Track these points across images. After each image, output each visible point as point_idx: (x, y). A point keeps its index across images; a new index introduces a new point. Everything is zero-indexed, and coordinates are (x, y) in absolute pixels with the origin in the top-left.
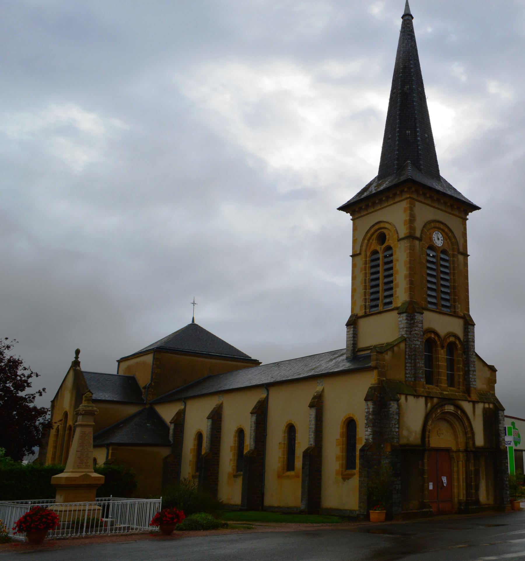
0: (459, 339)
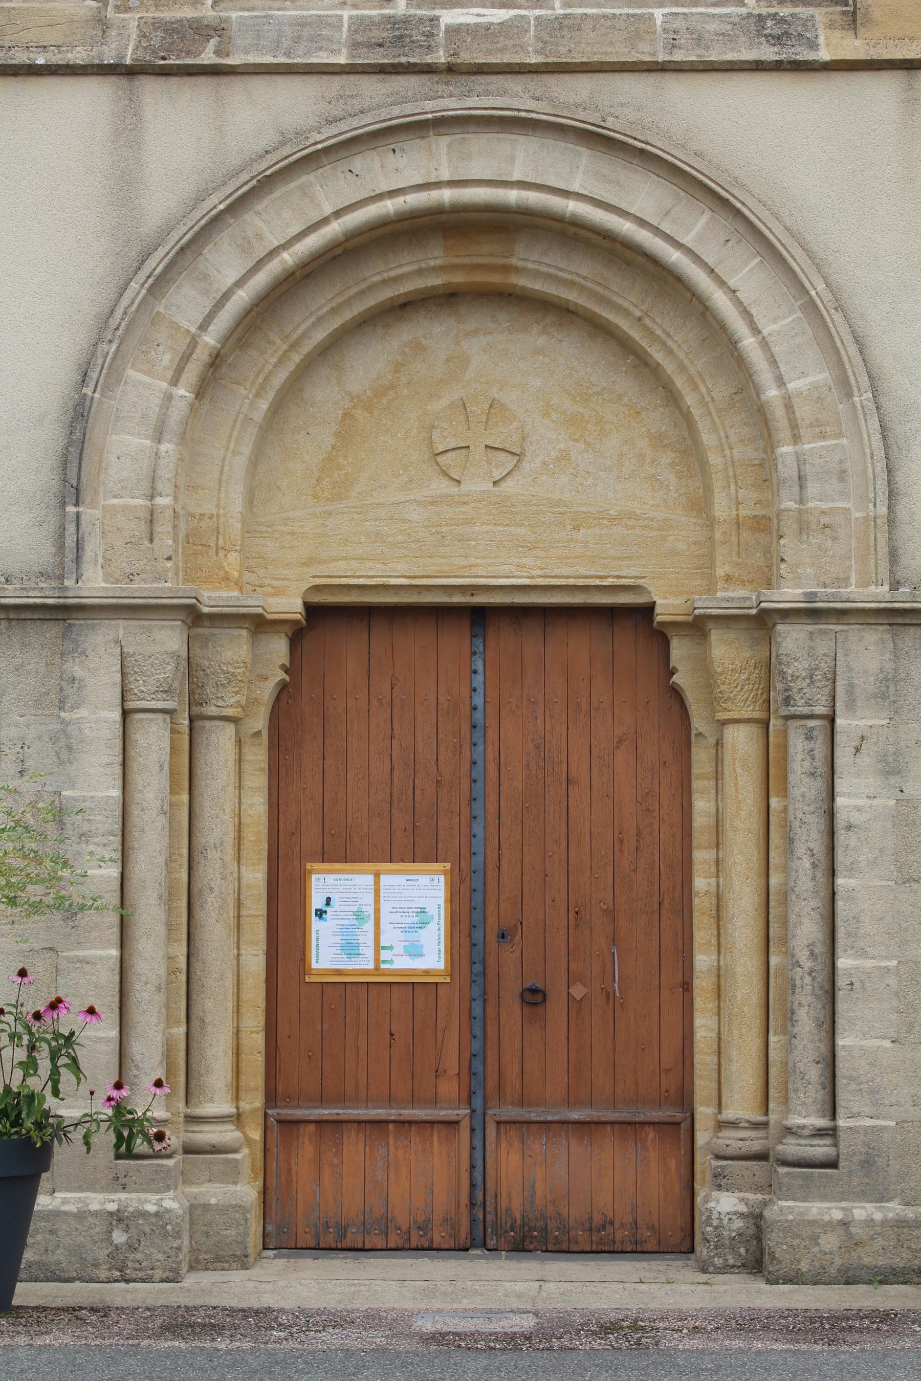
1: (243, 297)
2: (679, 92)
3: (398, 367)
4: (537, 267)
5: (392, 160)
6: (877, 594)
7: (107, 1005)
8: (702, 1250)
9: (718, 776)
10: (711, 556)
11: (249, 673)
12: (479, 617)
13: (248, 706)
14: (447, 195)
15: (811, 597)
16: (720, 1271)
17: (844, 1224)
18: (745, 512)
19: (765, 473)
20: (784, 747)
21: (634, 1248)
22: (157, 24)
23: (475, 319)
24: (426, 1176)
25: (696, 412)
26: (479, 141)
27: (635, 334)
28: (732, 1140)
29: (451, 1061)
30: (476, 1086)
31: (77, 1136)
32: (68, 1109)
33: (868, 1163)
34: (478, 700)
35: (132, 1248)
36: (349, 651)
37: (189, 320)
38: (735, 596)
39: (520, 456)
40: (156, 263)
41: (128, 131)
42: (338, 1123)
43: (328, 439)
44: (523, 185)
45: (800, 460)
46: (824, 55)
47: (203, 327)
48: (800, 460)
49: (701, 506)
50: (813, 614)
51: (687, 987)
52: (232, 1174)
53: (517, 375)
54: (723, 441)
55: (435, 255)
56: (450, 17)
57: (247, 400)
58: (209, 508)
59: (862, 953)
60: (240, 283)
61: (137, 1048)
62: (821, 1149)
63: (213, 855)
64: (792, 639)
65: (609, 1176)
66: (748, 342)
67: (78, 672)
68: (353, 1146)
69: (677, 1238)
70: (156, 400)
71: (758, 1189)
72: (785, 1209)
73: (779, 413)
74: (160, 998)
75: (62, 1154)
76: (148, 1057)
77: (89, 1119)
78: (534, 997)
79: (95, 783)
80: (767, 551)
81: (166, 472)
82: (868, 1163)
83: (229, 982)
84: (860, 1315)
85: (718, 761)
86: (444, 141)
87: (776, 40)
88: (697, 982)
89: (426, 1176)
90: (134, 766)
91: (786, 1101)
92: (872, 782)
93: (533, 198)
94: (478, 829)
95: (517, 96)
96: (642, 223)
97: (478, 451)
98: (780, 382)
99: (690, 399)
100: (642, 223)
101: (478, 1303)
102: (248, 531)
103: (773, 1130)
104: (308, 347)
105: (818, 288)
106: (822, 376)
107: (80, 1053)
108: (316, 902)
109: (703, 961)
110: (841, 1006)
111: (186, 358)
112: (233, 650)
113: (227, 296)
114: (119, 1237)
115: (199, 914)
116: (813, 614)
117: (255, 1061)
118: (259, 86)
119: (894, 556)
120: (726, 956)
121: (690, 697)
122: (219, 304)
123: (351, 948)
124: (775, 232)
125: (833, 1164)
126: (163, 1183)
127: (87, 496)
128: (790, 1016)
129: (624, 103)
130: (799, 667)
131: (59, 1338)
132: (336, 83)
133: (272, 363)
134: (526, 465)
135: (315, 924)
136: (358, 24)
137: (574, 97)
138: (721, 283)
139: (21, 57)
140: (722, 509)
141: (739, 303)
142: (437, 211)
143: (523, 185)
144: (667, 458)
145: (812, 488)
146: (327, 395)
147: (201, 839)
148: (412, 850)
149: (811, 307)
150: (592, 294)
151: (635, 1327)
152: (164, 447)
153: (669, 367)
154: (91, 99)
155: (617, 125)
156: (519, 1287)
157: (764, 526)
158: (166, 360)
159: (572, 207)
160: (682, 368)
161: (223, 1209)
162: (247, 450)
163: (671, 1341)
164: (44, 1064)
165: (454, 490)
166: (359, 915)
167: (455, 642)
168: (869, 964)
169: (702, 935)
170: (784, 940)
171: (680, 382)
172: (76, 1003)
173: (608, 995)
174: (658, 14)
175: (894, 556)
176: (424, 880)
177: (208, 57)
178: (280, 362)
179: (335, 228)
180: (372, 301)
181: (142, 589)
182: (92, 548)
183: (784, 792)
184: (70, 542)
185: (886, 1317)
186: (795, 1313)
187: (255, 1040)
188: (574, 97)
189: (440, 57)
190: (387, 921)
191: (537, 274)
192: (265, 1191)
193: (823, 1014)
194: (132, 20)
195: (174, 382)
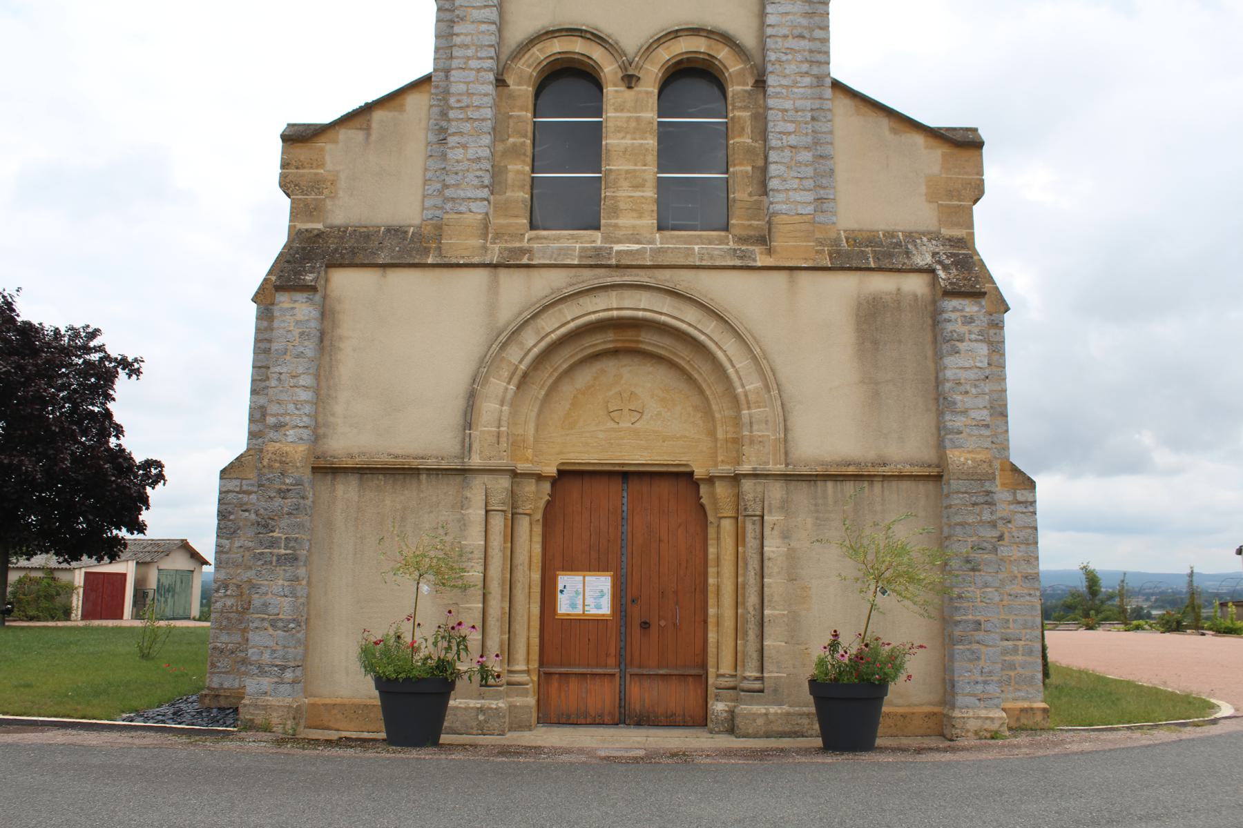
0: (726, 39)
1: (536, 350)
2: (704, 275)
3: (595, 379)
4: (650, 341)
5: (594, 300)
6: (780, 468)
7: (479, 624)
8: (710, 725)
9: (718, 539)
10: (716, 452)
11: (536, 496)
12: (625, 476)
13: (535, 509)
14: (615, 313)
15: (755, 469)
16: (717, 733)
17: (766, 714)
18: (729, 436)
19: (737, 421)
20: (744, 528)
21: (684, 724)
22: (506, 249)
23: (625, 360)
24: (602, 695)
25: (710, 397)
26: (627, 293)
27: (687, 367)
28: (722, 682)
29: (612, 650)
30: (622, 660)
31: (466, 677)
32: (462, 667)
33: (775, 690)
34: (625, 508)
35: (486, 721)
36: (574, 489)
37: (515, 360)
38: (725, 469)
39: (642, 413)
40: (503, 338)
41: (494, 288)
42: (567, 674)
43: (568, 406)
44: (644, 310)
45: (750, 416)
46: (759, 264)
47: (520, 362)
48: (750, 416)
49: (712, 433)
50: (756, 476)
51: (705, 622)
52: (525, 693)
53: (641, 382)
54: (721, 409)
55: (610, 336)
56: (617, 247)
57: (537, 390)
58: (521, 432)
59: (774, 608)
60: (535, 346)
61: (489, 643)
62: (757, 685)
63: (520, 568)
64: (747, 485)
65: (675, 696)
66: (731, 371)
67: (469, 495)
68: (573, 684)
69: (701, 720)
70: (502, 390)
71: (732, 701)
72: (743, 708)
73: (742, 398)
74: (498, 624)
75: (458, 683)
76: (494, 645)
77: (470, 670)
78: (645, 625)
79: (475, 539)
80: (738, 451)
81: (504, 418)
82: (775, 690)
83: (526, 618)
84: (772, 750)
85: (718, 533)
86: (614, 293)
87: (741, 258)
88: (709, 620)
89: (602, 695)
90: (490, 532)
91: (744, 666)
92: (778, 541)
93: (648, 315)
94: (624, 559)
95: (630, 277)
96: (690, 325)
97: (626, 411)
98: (743, 386)
99: (708, 392)
100: (690, 325)
101: (623, 745)
102: (536, 440)
103: (739, 678)
104: (561, 370)
105: (757, 351)
106: (759, 384)
107: (469, 644)
108: (560, 587)
109: (712, 611)
110: (765, 629)
111: (513, 374)
112: (529, 487)
113: (530, 350)
114: (481, 717)
115: (514, 591)
116: (756, 476)
117: (535, 649)
118: (544, 271)
119: (786, 454)
120: (721, 610)
121: (708, 508)
122: (527, 354)
123: (573, 606)
124: (741, 330)
125: (762, 691)
126: (497, 696)
127: (474, 426)
128: (746, 633)
129: (683, 281)
130: (750, 496)
131: (458, 756)
132: (574, 270)
133: (546, 376)
134: (644, 417)
135: (560, 596)
136: (583, 249)
137: (664, 278)
138: (720, 348)
139: (454, 261)
140: (720, 434)
141: (727, 356)
142: (611, 319)
143: (644, 310)
144: (699, 415)
145: (755, 427)
146: (567, 389)
147: (516, 562)
148: (596, 566)
149: (754, 358)
150: (670, 351)
151: (684, 754)
152: (504, 408)
153: (700, 380)
154: (481, 275)
155: (681, 288)
156: (639, 739)
157: (737, 441)
158: (506, 374)
159: (663, 318)
160: (705, 380)
161: (521, 707)
162: (536, 410)
163: (699, 760)
164: (455, 648)
165: (616, 426)
166: (577, 592)
167: (616, 486)
168: (776, 612)
169: (712, 601)
170: (744, 603)
171: (704, 386)
172: (468, 622)
173: (675, 624)
174: (696, 247)
175: (786, 454)
176: (603, 579)
177: (525, 261)
178: (550, 375)
179: (572, 325)
180: (586, 353)
181: (494, 463)
182: (476, 446)
183: (744, 546)
184: (467, 445)
185: (782, 750)
186: (747, 749)
187: (535, 641)
188: (664, 278)
189: (613, 262)
190: (588, 594)
191: (650, 344)
192: (538, 700)
193: (759, 632)
194: (496, 247)
195: (509, 383)
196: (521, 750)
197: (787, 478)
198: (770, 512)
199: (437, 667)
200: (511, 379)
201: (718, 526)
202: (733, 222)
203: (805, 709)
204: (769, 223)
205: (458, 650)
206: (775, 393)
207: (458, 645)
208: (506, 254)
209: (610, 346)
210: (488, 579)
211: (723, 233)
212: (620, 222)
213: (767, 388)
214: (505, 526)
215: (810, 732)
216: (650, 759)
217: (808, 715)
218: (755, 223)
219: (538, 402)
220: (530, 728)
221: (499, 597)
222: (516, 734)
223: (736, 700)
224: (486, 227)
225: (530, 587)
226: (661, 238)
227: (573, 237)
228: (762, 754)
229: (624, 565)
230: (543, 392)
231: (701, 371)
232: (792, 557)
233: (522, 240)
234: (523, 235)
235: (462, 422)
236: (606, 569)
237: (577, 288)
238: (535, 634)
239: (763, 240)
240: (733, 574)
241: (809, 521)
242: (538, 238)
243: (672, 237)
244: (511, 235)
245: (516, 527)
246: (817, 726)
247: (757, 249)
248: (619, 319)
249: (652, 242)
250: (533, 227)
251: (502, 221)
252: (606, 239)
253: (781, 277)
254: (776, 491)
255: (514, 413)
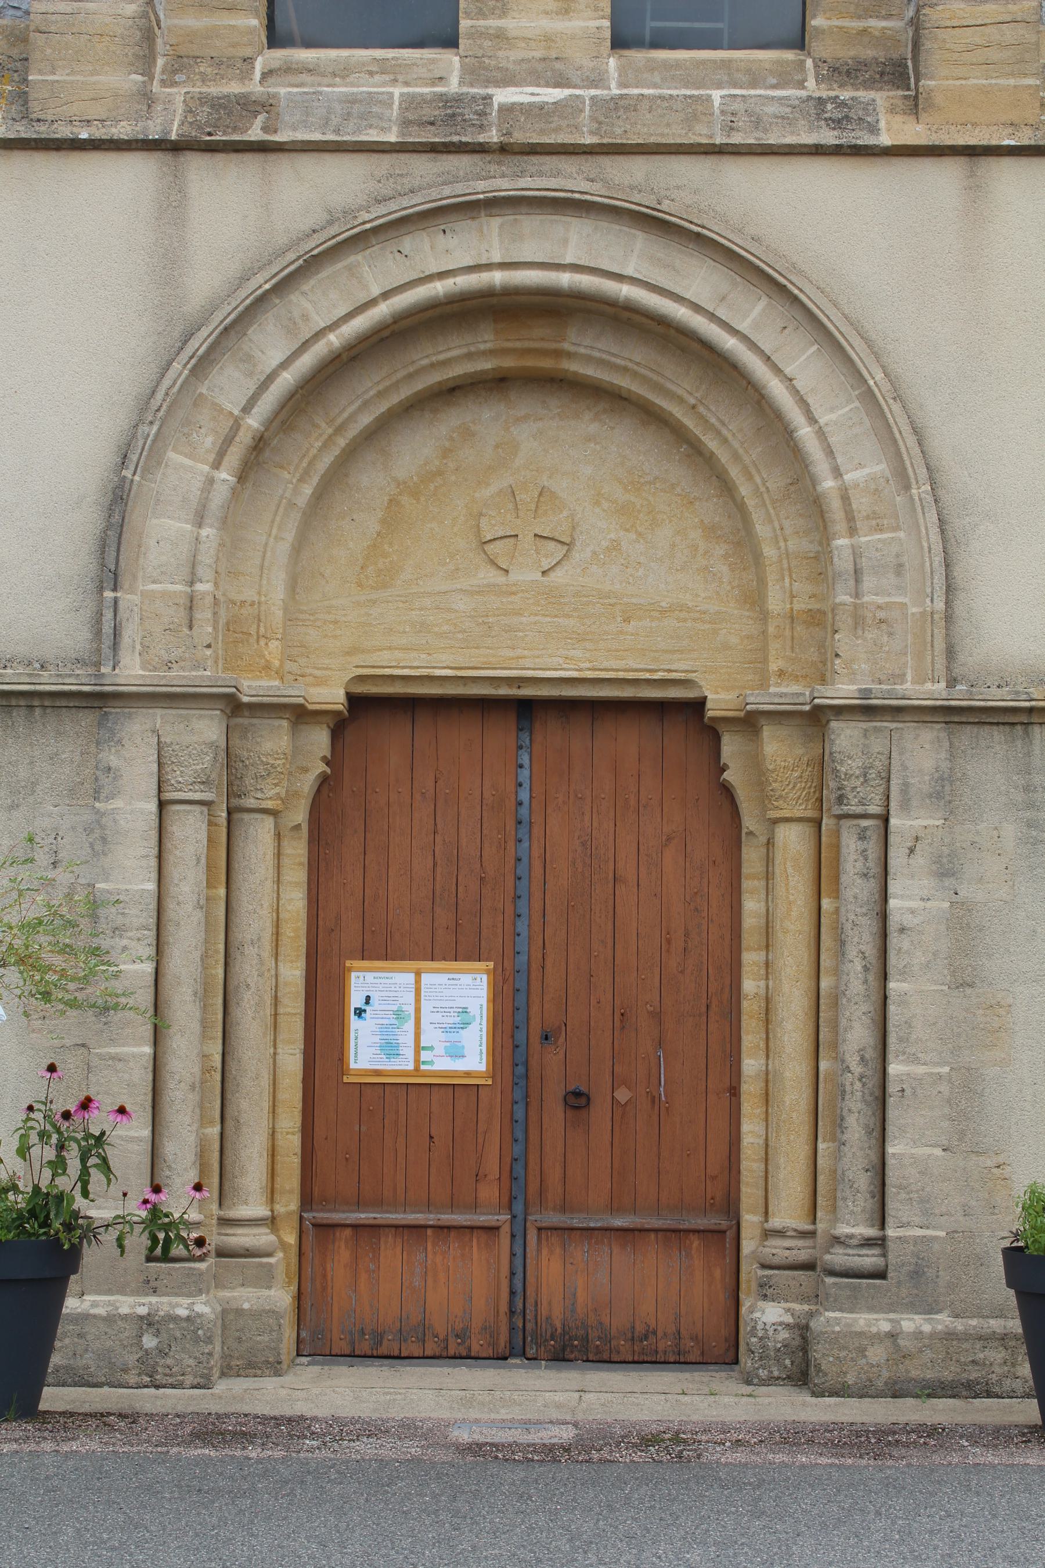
1: (288, 378)
2: (735, 174)
3: (446, 453)
4: (589, 352)
5: (450, 241)
6: (932, 691)
7: (139, 1103)
8: (746, 1362)
9: (768, 876)
10: (764, 649)
11: (290, 765)
12: (525, 710)
14: (498, 278)
15: (866, 694)
17: (892, 1336)
18: (799, 606)
19: (820, 566)
20: (837, 847)
22: (203, 99)
23: (524, 404)
24: (464, 1282)
25: (751, 503)
26: (530, 222)
27: (689, 422)
28: (778, 1250)
29: (492, 1166)
30: (517, 1192)
31: (109, 1237)
33: (916, 1274)
34: (524, 795)
35: (162, 1353)
38: (788, 692)
39: (569, 545)
40: (199, 343)
41: (172, 209)
42: (375, 1228)
44: (576, 268)
46: (885, 140)
47: (247, 409)
48: (856, 553)
49: (754, 599)
50: (868, 711)
51: (734, 1092)
52: (266, 1278)
53: (569, 464)
54: (778, 533)
55: (485, 338)
56: (503, 96)
57: (291, 486)
58: (249, 594)
59: (915, 1060)
60: (284, 365)
61: (170, 1148)
62: (869, 1259)
63: (250, 951)
64: (845, 736)
65: (653, 1285)
66: (805, 432)
67: (114, 761)
68: (391, 1253)
69: (721, 1349)
70: (197, 484)
71: (804, 1299)
72: (832, 1320)
73: (835, 505)
74: (193, 1098)
75: (91, 1256)
76: (181, 1173)
77: (120, 1220)
78: (577, 1101)
79: (131, 877)
80: (821, 646)
81: (206, 557)
82: (916, 1274)
83: (265, 1081)
84: (907, 1429)
85: (769, 860)
86: (496, 222)
87: (837, 124)
88: (745, 1087)
89: (464, 1282)
90: (170, 859)
91: (834, 1209)
92: (926, 884)
93: (586, 282)
94: (522, 926)
95: (571, 178)
96: (697, 308)
97: (527, 540)
98: (837, 473)
99: (744, 490)
100: (697, 308)
101: (517, 1413)
102: (290, 618)
103: (820, 1239)
104: (354, 430)
105: (876, 377)
106: (880, 468)
108: (356, 1000)
109: (751, 1065)
110: (892, 1114)
111: (228, 441)
112: (273, 741)
113: (271, 378)
114: (149, 1342)
115: (236, 1012)
116: (868, 711)
118: (307, 163)
119: (950, 653)
120: (776, 1060)
121: (742, 794)
123: (390, 1048)
124: (834, 320)
126: (195, 1287)
127: (125, 581)
128: (839, 1123)
130: (852, 766)
131: (86, 1444)
132: (386, 161)
133: (316, 446)
134: (576, 555)
136: (410, 102)
137: (629, 179)
138: (778, 371)
139: (64, 132)
140: (775, 602)
141: (795, 392)
142: (488, 294)
143: (576, 268)
144: (720, 550)
145: (869, 582)
146: (372, 481)
147: (237, 935)
148: (452, 947)
149: (869, 397)
150: (645, 380)
151: (676, 1439)
152: (205, 532)
153: (723, 456)
154: (137, 173)
155: (672, 208)
156: (559, 1397)
157: (820, 620)
158: (208, 442)
159: (626, 291)
160: (736, 457)
161: (256, 1315)
163: (713, 1455)
164: (74, 1165)
166: (399, 1014)
167: (500, 735)
168: (921, 1070)
169: (750, 1038)
170: (835, 1045)
171: (734, 472)
173: (654, 1100)
174: (716, 95)
175: (950, 653)
176: (466, 979)
177: (255, 133)
178: (325, 446)
179: (383, 310)
182: (130, 633)
183: (836, 894)
184: (107, 628)
185: (932, 1431)
186: (840, 1426)
187: (291, 1142)
188: (629, 179)
189: (493, 136)
190: (428, 1020)
191: (589, 359)
192: (299, 1296)
193: (874, 1122)
194: (177, 95)
195: (217, 465)
196: (250, 1427)
197: (951, 716)
198: (905, 805)
199: (33, 1213)
200: (221, 454)
201: (770, 843)
202: (817, 22)
203: (995, 1325)
204: (916, 24)
205: (85, 1172)
206: (921, 490)
207: (84, 1160)
208: (203, 114)
209: (486, 365)
210: (167, 981)
211: (789, 55)
212: (511, 24)
213: (902, 478)
214: (210, 840)
215: (1007, 1383)
216: (587, 1451)
217: (1003, 1338)
218: (875, 24)
219: (296, 516)
220: (276, 1368)
221: (196, 1027)
222: (238, 1385)
223: (815, 1297)
224: (149, 37)
225: (276, 1001)
226: (622, 70)
227: (383, 67)
228: (880, 1441)
229: (522, 944)
230: (308, 490)
231: (727, 433)
232: (962, 922)
233: (246, 75)
234: (249, 61)
235: (93, 567)
236: (474, 955)
237: (395, 208)
238: (290, 1122)
239: (899, 73)
240: (807, 1045)
241: (1010, 831)
242: (288, 69)
243: (652, 67)
244: (216, 62)
245: (239, 843)
246: (1025, 1370)
247: (881, 98)
248: (510, 291)
249: (597, 81)
250: (275, 38)
251: (192, 21)
252: (473, 73)
253: (946, 174)
254: (921, 752)
255: (232, 542)
